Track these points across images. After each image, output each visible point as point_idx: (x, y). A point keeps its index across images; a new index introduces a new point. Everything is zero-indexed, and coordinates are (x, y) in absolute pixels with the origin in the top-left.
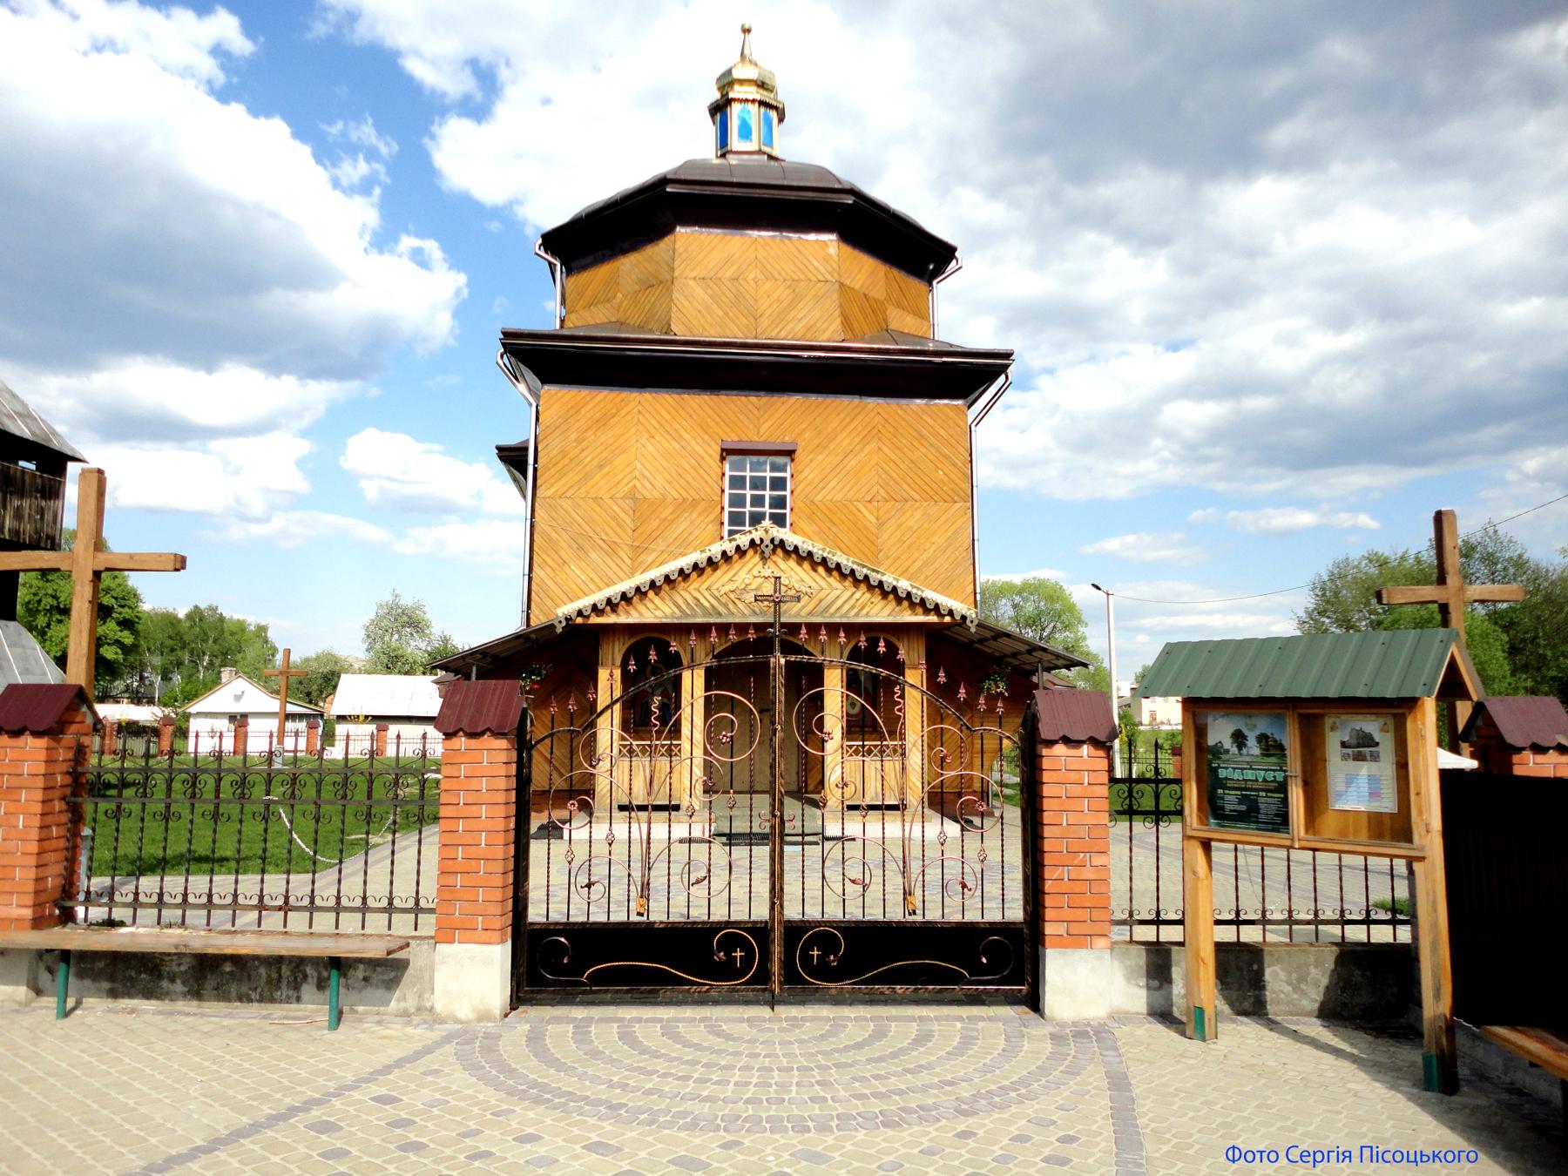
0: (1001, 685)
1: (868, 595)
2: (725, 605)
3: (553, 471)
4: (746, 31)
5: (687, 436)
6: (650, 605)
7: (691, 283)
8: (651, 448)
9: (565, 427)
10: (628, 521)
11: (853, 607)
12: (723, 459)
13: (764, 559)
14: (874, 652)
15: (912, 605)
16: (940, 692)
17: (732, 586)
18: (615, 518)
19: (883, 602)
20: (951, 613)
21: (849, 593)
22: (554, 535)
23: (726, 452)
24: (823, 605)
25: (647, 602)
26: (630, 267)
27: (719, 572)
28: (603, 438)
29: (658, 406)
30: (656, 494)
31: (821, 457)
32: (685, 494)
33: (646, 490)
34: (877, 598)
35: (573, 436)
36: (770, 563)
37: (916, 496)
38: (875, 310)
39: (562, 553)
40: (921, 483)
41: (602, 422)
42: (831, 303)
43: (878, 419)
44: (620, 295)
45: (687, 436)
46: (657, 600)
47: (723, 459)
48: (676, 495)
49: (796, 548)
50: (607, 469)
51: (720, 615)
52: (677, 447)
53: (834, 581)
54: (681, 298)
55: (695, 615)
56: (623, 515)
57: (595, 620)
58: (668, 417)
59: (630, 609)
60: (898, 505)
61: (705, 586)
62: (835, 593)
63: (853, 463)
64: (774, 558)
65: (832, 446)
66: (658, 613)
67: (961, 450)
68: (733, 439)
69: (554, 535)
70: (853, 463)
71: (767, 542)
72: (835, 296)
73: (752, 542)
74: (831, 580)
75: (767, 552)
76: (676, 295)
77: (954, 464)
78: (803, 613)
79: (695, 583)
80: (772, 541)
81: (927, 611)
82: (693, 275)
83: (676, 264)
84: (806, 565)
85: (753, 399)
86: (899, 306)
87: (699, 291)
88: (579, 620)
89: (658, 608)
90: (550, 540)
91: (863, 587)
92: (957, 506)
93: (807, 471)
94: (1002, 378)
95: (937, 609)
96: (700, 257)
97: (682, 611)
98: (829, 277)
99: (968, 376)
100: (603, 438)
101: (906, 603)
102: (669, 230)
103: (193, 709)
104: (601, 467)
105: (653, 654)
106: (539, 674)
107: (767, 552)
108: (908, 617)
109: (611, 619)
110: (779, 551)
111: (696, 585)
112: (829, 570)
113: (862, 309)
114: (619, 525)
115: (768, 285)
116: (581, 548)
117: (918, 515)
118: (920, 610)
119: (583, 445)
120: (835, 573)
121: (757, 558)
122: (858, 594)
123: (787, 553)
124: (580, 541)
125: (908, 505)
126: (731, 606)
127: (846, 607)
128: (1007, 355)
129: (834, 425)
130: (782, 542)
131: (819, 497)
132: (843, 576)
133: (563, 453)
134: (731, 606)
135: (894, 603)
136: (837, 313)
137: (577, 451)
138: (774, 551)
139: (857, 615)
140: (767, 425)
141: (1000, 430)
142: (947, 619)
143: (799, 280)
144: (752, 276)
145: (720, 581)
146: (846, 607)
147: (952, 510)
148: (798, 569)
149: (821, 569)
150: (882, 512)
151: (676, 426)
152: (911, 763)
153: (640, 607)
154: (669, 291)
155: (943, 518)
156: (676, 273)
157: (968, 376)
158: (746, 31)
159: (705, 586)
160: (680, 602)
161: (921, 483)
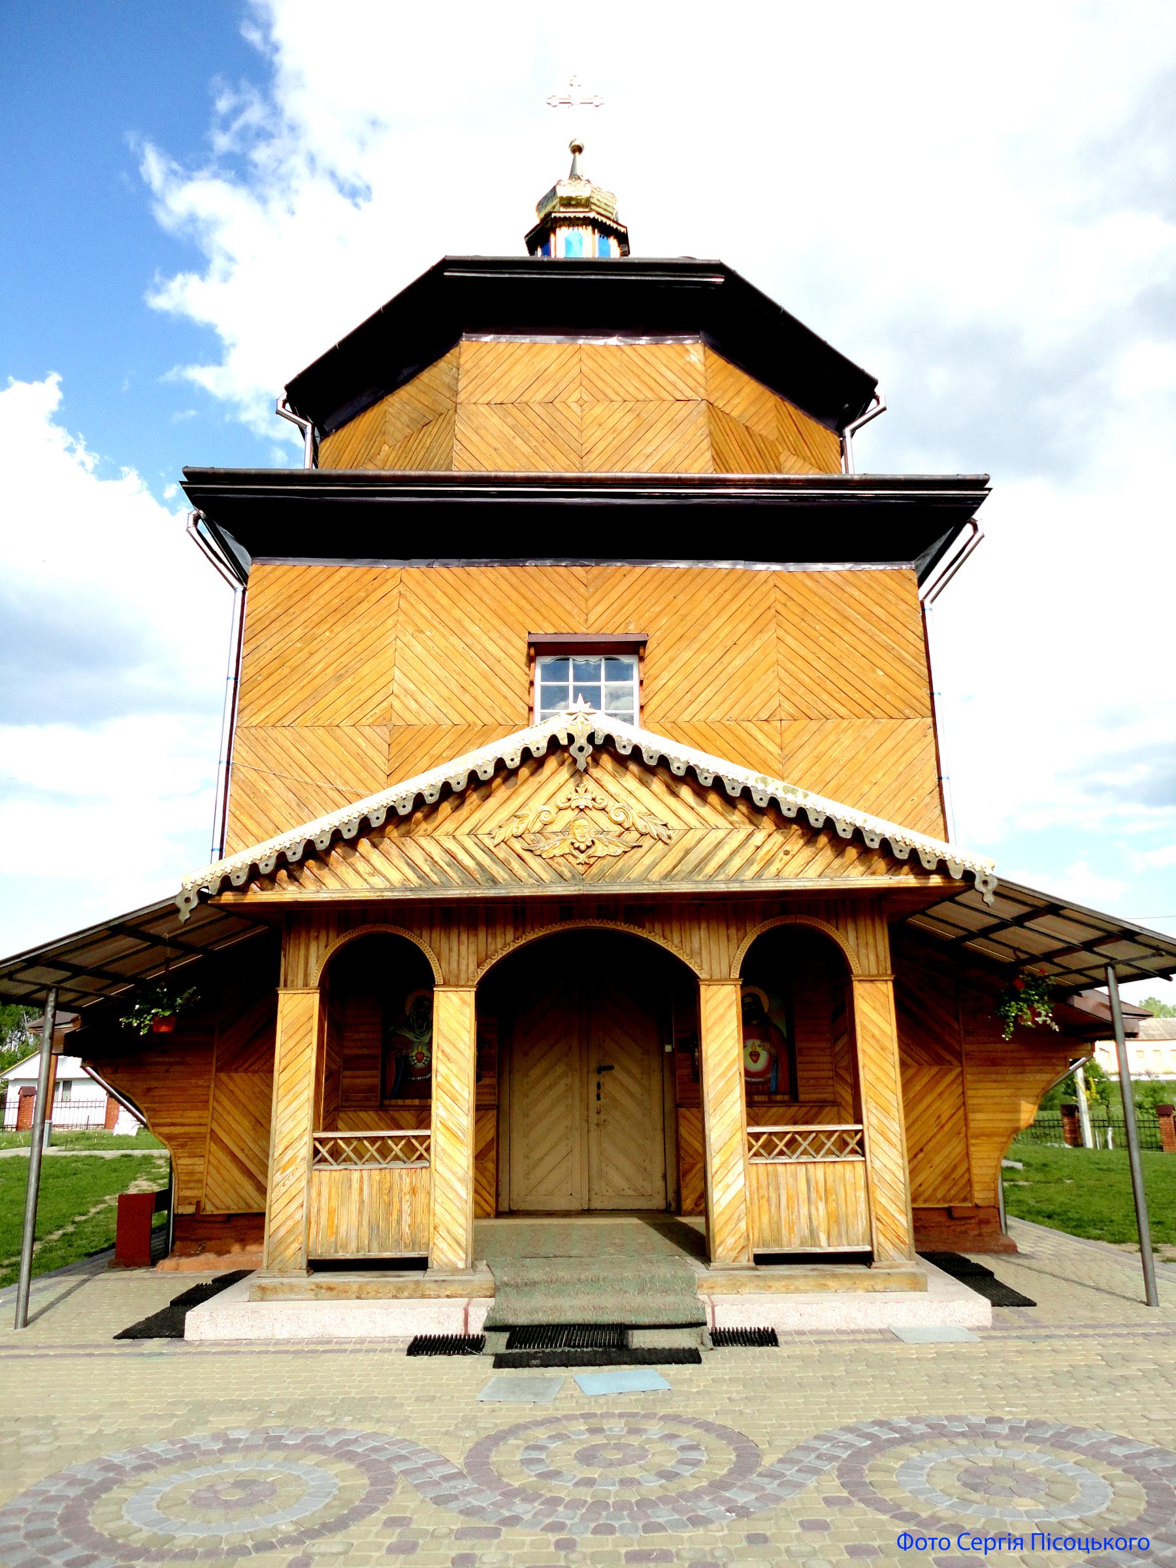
0: (1042, 1009)
1: (778, 838)
2: (504, 864)
3: (264, 686)
4: (577, 149)
5: (474, 629)
6: (362, 866)
7: (484, 409)
8: (419, 649)
9: (285, 619)
10: (380, 760)
11: (749, 862)
12: (531, 660)
13: (578, 774)
14: (794, 958)
15: (865, 852)
16: (920, 1035)
17: (516, 827)
18: (360, 757)
19: (808, 852)
20: (942, 867)
21: (740, 836)
22: (262, 786)
23: (538, 649)
24: (693, 858)
25: (356, 859)
26: (399, 407)
27: (492, 802)
28: (343, 636)
29: (429, 585)
30: (425, 719)
31: (687, 655)
32: (471, 718)
33: (408, 710)
34: (796, 843)
35: (298, 633)
36: (588, 782)
37: (842, 711)
38: (765, 453)
39: (274, 813)
40: (848, 689)
41: (341, 612)
42: (697, 429)
43: (775, 594)
44: (386, 448)
45: (474, 629)
46: (375, 857)
47: (531, 660)
48: (457, 719)
49: (637, 750)
50: (348, 682)
51: (494, 881)
52: (460, 645)
53: (711, 812)
54: (469, 432)
55: (444, 886)
56: (371, 752)
57: (257, 895)
58: (445, 601)
59: (325, 874)
60: (813, 725)
61: (466, 828)
62: (714, 837)
63: (738, 662)
64: (595, 772)
65: (704, 636)
66: (377, 882)
67: (911, 637)
68: (546, 631)
69: (262, 786)
70: (738, 662)
71: (581, 741)
72: (702, 420)
73: (553, 741)
74: (705, 811)
75: (582, 760)
76: (460, 427)
77: (901, 660)
78: (655, 875)
79: (447, 820)
80: (591, 738)
81: (895, 865)
82: (486, 399)
83: (461, 385)
84: (657, 785)
85: (578, 570)
86: (796, 453)
87: (495, 420)
88: (228, 897)
89: (376, 871)
90: (252, 791)
91: (767, 823)
92: (911, 723)
93: (665, 676)
94: (968, 529)
95: (914, 860)
96: (496, 375)
97: (423, 876)
98: (690, 394)
99: (920, 522)
100: (343, 636)
101: (852, 852)
102: (449, 342)
103: (11, 1076)
104: (339, 678)
105: (379, 967)
106: (171, 1006)
107: (582, 760)
108: (858, 877)
109: (287, 893)
110: (606, 760)
111: (448, 826)
112: (701, 792)
113: (742, 446)
114: (365, 768)
115: (598, 409)
116: (302, 803)
117: (846, 740)
118: (880, 864)
119: (314, 646)
120: (713, 798)
121: (565, 773)
122: (759, 837)
123: (621, 761)
124: (303, 794)
125: (830, 725)
126: (516, 865)
127: (737, 862)
128: (980, 484)
129: (706, 604)
130: (609, 739)
131: (686, 716)
132: (730, 802)
133: (281, 660)
134: (516, 865)
135: (828, 853)
136: (706, 444)
137: (303, 655)
138: (596, 761)
139: (758, 876)
140: (600, 609)
141: (972, 598)
142: (935, 880)
143: (647, 401)
144: (576, 396)
145: (494, 816)
146: (737, 862)
147: (903, 730)
148: (641, 791)
149: (685, 792)
150: (788, 735)
151: (457, 613)
152: (871, 1178)
153: (344, 871)
154: (452, 424)
155: (889, 744)
156: (461, 397)
157: (920, 522)
158: (577, 149)
159: (466, 828)
160: (418, 858)
161: (848, 689)
